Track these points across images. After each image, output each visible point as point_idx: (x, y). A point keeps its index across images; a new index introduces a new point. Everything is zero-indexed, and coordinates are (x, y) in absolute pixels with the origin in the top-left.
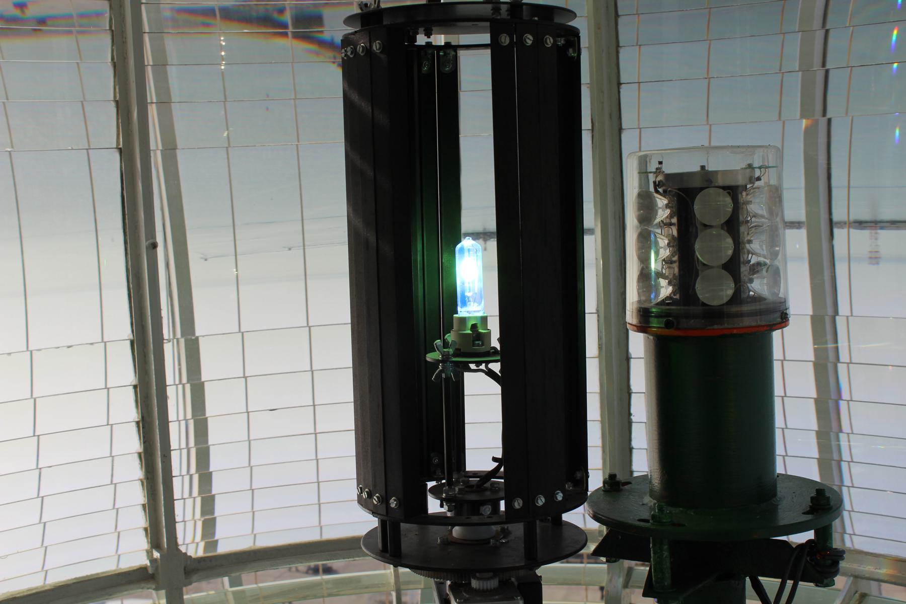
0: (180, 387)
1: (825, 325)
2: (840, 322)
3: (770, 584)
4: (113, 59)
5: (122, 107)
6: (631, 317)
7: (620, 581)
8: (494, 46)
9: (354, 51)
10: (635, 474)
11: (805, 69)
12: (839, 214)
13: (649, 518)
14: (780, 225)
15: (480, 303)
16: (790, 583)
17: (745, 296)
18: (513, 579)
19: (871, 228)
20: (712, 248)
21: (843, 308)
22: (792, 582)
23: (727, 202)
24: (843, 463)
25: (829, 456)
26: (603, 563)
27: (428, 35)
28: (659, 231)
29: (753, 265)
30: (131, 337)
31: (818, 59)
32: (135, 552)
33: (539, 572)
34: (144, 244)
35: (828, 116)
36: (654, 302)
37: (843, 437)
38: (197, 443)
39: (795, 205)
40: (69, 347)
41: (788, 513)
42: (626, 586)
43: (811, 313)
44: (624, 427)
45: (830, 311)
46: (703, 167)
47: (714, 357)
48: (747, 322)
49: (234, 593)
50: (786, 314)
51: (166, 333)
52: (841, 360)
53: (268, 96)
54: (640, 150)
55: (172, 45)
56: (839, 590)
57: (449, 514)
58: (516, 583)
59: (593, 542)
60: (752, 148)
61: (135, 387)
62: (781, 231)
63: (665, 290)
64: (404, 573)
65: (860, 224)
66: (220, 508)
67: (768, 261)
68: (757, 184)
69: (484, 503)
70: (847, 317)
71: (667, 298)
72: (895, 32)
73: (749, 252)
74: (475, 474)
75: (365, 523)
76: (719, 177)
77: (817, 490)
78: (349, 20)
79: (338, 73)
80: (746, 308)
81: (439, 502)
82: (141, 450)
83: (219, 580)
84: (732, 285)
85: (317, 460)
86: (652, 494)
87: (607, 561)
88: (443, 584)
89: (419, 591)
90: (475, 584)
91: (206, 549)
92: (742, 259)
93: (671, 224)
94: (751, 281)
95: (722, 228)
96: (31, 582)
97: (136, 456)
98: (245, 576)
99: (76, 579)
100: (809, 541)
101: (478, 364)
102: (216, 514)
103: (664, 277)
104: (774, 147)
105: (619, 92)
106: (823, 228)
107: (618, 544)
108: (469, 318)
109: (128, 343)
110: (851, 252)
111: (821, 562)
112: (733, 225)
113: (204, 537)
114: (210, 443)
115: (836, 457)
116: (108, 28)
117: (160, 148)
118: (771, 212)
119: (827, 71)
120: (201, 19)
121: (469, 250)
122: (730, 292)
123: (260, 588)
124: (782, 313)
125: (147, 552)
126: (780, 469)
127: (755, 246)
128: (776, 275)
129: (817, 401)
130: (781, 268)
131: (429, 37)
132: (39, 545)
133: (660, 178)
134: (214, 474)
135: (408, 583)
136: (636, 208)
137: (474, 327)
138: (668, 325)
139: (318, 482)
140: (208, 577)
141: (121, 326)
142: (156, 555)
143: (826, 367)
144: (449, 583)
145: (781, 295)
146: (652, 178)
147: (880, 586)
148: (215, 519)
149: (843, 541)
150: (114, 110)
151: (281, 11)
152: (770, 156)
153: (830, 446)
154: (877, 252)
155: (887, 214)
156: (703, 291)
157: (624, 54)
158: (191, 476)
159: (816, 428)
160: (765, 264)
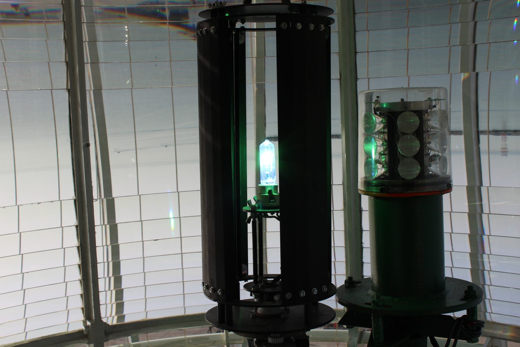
0: (104, 226)
1: (474, 191)
2: (484, 190)
3: (441, 340)
4: (64, 37)
5: (70, 65)
6: (361, 186)
7: (356, 339)
8: (278, 29)
9: (201, 32)
10: (365, 277)
11: (463, 44)
12: (483, 126)
13: (371, 302)
14: (447, 133)
15: (273, 178)
16: (452, 340)
17: (427, 174)
18: (292, 338)
19: (502, 134)
20: (408, 146)
21: (485, 181)
22: (454, 340)
23: (415, 120)
24: (485, 272)
25: (477, 267)
26: (344, 329)
27: (243, 22)
28: (377, 136)
29: (431, 156)
30: (75, 198)
31: (470, 38)
32: (76, 322)
33: (307, 333)
34: (82, 144)
35: (477, 71)
36: (374, 177)
37: (485, 257)
38: (113, 259)
39: (457, 122)
40: (39, 203)
41: (451, 300)
42: (359, 342)
43: (467, 185)
44: (351, 249)
45: (478, 184)
46: (402, 100)
47: (409, 206)
48: (428, 189)
49: (134, 345)
50: (451, 185)
51: (95, 195)
52: (484, 211)
53: (156, 58)
54: (369, 90)
55: (100, 30)
56: (482, 345)
57: (255, 300)
58: (294, 340)
59: (340, 317)
60: (431, 89)
61: (77, 227)
62: (447, 136)
63: (380, 170)
64: (231, 334)
65: (496, 132)
66: (126, 297)
67: (440, 154)
68: (434, 109)
69: (275, 293)
70: (488, 187)
71: (382, 175)
72: (516, 21)
73: (429, 149)
74: (271, 276)
75: (206, 305)
76: (412, 105)
77: (468, 287)
78: (201, 14)
79: (194, 44)
80: (427, 181)
81: (249, 293)
82: (80, 263)
83: (126, 338)
84: (419, 168)
85: (183, 269)
86: (373, 288)
87: (347, 327)
88: (253, 340)
89: (241, 345)
90: (270, 340)
91: (118, 320)
92: (425, 153)
93: (384, 133)
94: (430, 166)
95: (413, 135)
96: (21, 339)
97: (77, 266)
98: (140, 336)
99: (42, 337)
100: (464, 316)
101: (272, 213)
102: (124, 300)
103: (380, 163)
104: (443, 88)
105: (356, 58)
106: (473, 136)
107: (353, 318)
108: (267, 186)
109: (73, 201)
110: (490, 149)
111: (472, 327)
112: (420, 133)
113: (117, 313)
114: (121, 259)
115: (481, 268)
116: (62, 20)
117: (93, 89)
118: (441, 125)
119: (476, 46)
120: (118, 14)
121: (267, 147)
122: (418, 172)
123: (150, 343)
124: (448, 184)
125: (83, 321)
126: (448, 274)
127: (432, 145)
128: (444, 162)
129: (470, 236)
130: (447, 158)
131: (243, 24)
132: (23, 317)
133: (377, 106)
134: (123, 277)
135: (235, 340)
136: (363, 123)
137: (270, 192)
138: (382, 191)
139: (183, 282)
140: (119, 336)
141: (69, 192)
142: (89, 323)
143: (475, 216)
144: (255, 340)
145: (447, 174)
146: (373, 106)
147: (507, 343)
148: (123, 303)
149: (485, 316)
150: (65, 67)
151: (164, 9)
152: (441, 93)
153: (478, 261)
154: (505, 148)
155: (512, 126)
156: (401, 171)
157: (358, 35)
158: (110, 278)
159: (470, 251)
160: (438, 156)
